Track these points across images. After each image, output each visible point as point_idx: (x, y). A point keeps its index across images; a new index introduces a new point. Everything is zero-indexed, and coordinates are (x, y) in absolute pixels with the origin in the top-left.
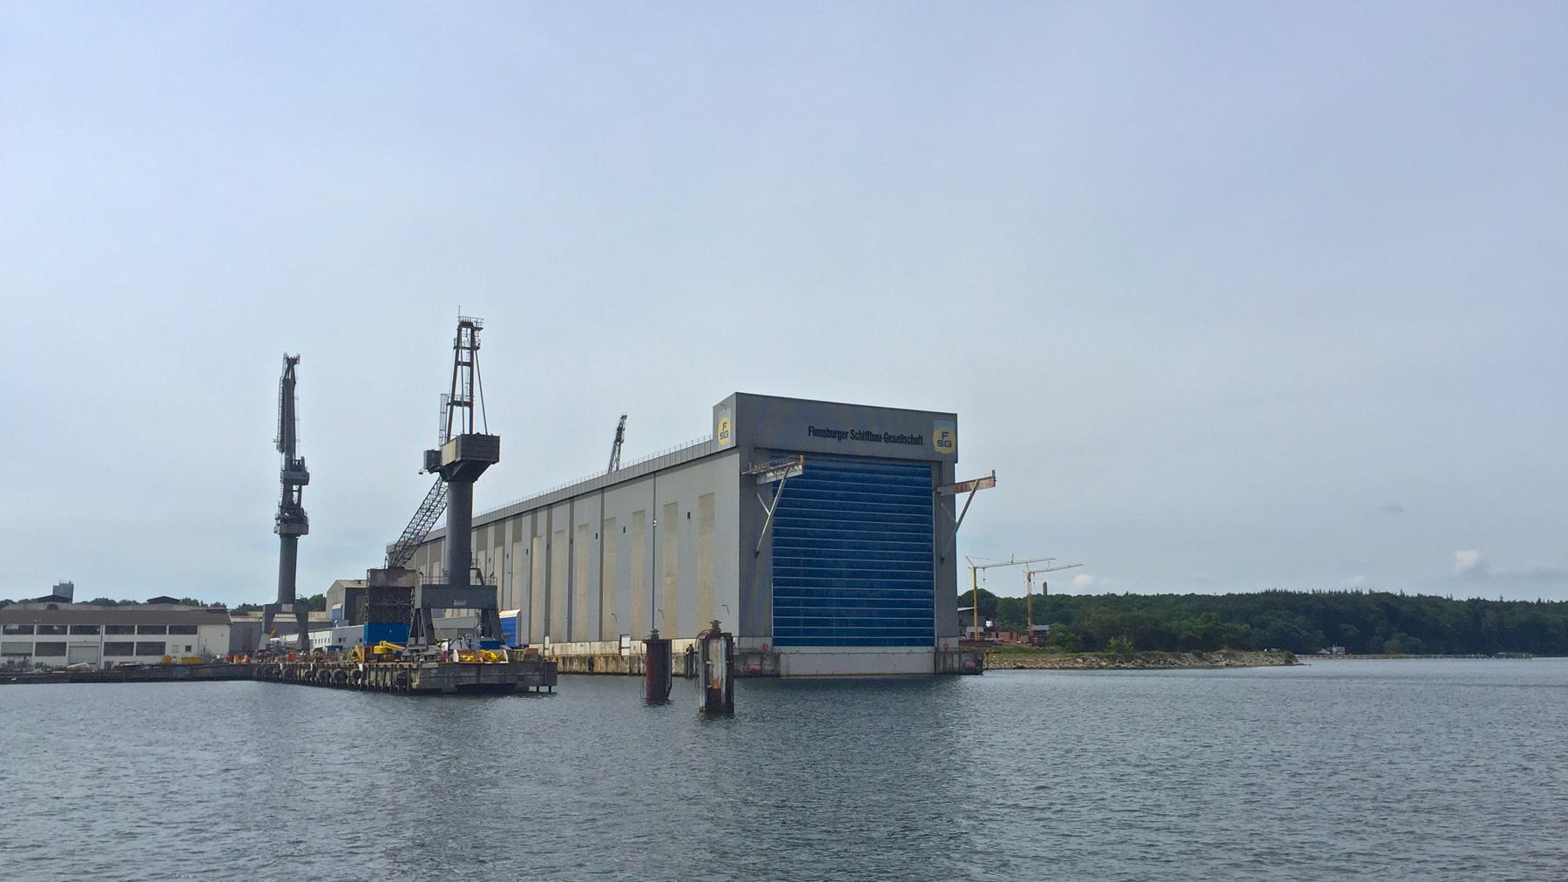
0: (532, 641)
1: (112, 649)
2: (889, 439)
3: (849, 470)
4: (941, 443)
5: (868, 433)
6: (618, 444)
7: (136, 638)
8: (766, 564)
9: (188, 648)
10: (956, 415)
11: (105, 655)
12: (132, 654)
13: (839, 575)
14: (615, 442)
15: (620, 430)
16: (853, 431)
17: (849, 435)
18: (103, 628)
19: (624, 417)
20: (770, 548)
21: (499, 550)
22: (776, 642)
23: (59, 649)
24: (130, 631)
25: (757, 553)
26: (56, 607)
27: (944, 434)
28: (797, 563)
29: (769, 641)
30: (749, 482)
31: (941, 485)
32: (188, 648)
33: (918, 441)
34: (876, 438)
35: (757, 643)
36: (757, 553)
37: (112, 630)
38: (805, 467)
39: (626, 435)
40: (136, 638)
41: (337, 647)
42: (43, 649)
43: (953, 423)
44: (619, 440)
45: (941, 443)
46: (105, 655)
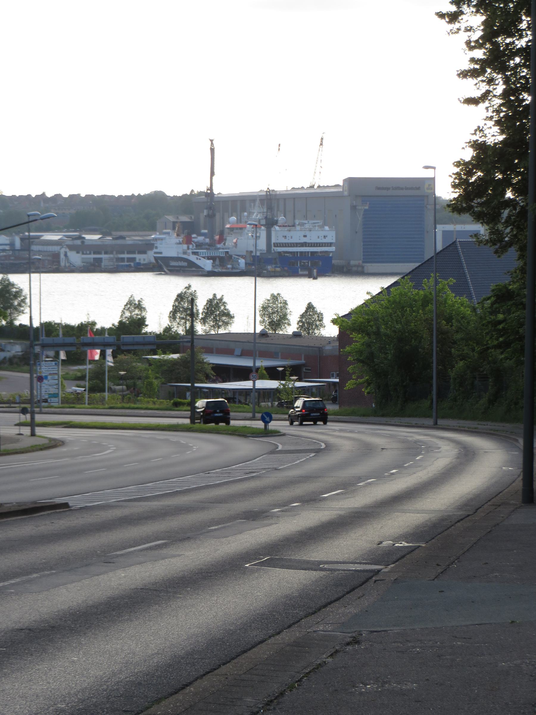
4: (428, 189)
7: (126, 256)
16: (392, 187)
18: (103, 252)
22: (363, 262)
24: (123, 253)
25: (356, 232)
27: (429, 185)
29: (361, 262)
30: (354, 208)
31: (428, 204)
34: (402, 189)
36: (356, 232)
37: (128, 253)
40: (126, 256)
45: (428, 189)
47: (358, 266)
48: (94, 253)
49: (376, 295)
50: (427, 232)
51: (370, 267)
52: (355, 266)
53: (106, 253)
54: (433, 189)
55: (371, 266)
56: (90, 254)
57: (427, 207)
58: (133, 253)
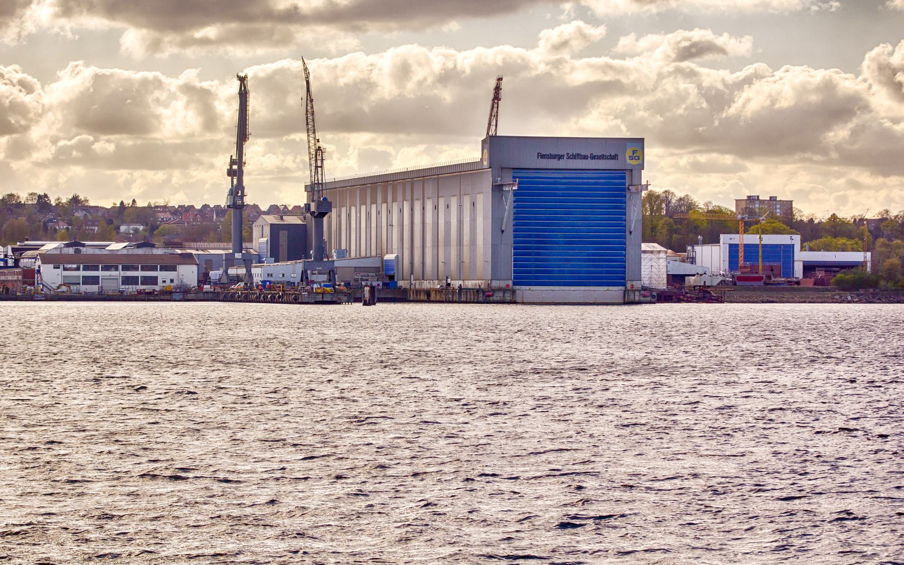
0: (425, 278)
1: (127, 281)
2: (593, 157)
3: (566, 178)
5: (578, 155)
6: (496, 101)
7: (139, 274)
8: (509, 237)
9: (172, 281)
10: (643, 140)
11: (122, 284)
12: (138, 284)
13: (558, 243)
14: (493, 100)
15: (498, 89)
17: (566, 157)
18: (120, 267)
19: (500, 79)
20: (511, 228)
21: (384, 206)
22: (515, 284)
23: (95, 280)
24: (136, 269)
25: (503, 231)
26: (80, 251)
28: (530, 236)
29: (510, 283)
31: (632, 185)
32: (172, 281)
33: (614, 157)
34: (585, 157)
35: (503, 284)
36: (503, 231)
37: (125, 268)
38: (518, 187)
39: (503, 93)
40: (139, 274)
41: (268, 281)
42: (87, 280)
43: (641, 144)
44: (497, 98)
45: (631, 158)
46: (122, 284)
47: (504, 290)
48: (86, 268)
49: (859, 251)
50: (631, 233)
51: (525, 291)
52: (500, 289)
53: (106, 268)
54: (641, 158)
55: (530, 289)
56: (78, 269)
57: (629, 189)
58: (154, 268)
